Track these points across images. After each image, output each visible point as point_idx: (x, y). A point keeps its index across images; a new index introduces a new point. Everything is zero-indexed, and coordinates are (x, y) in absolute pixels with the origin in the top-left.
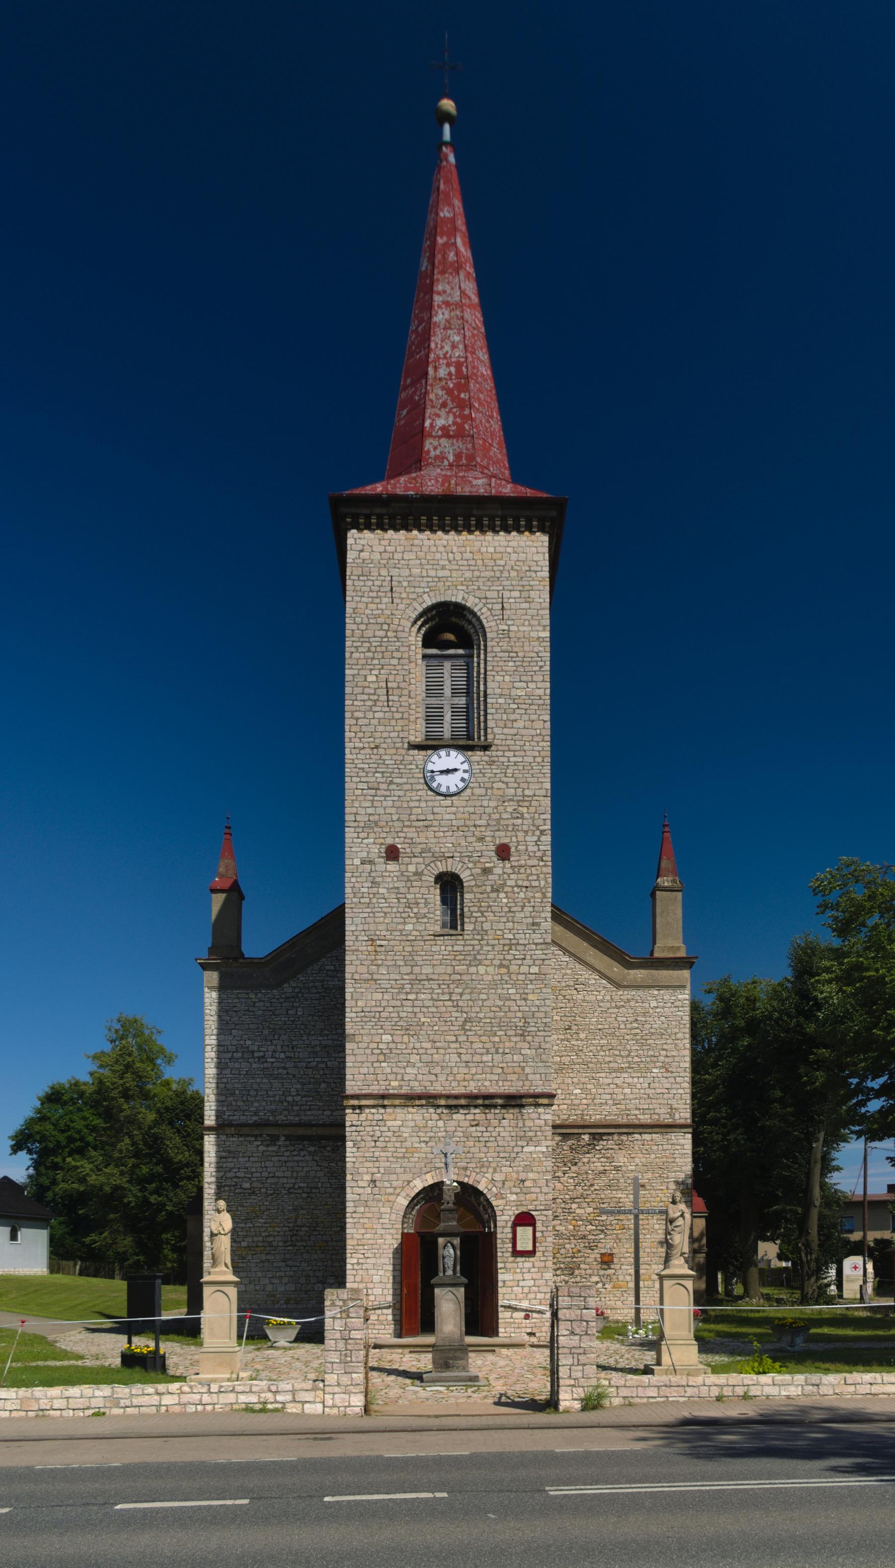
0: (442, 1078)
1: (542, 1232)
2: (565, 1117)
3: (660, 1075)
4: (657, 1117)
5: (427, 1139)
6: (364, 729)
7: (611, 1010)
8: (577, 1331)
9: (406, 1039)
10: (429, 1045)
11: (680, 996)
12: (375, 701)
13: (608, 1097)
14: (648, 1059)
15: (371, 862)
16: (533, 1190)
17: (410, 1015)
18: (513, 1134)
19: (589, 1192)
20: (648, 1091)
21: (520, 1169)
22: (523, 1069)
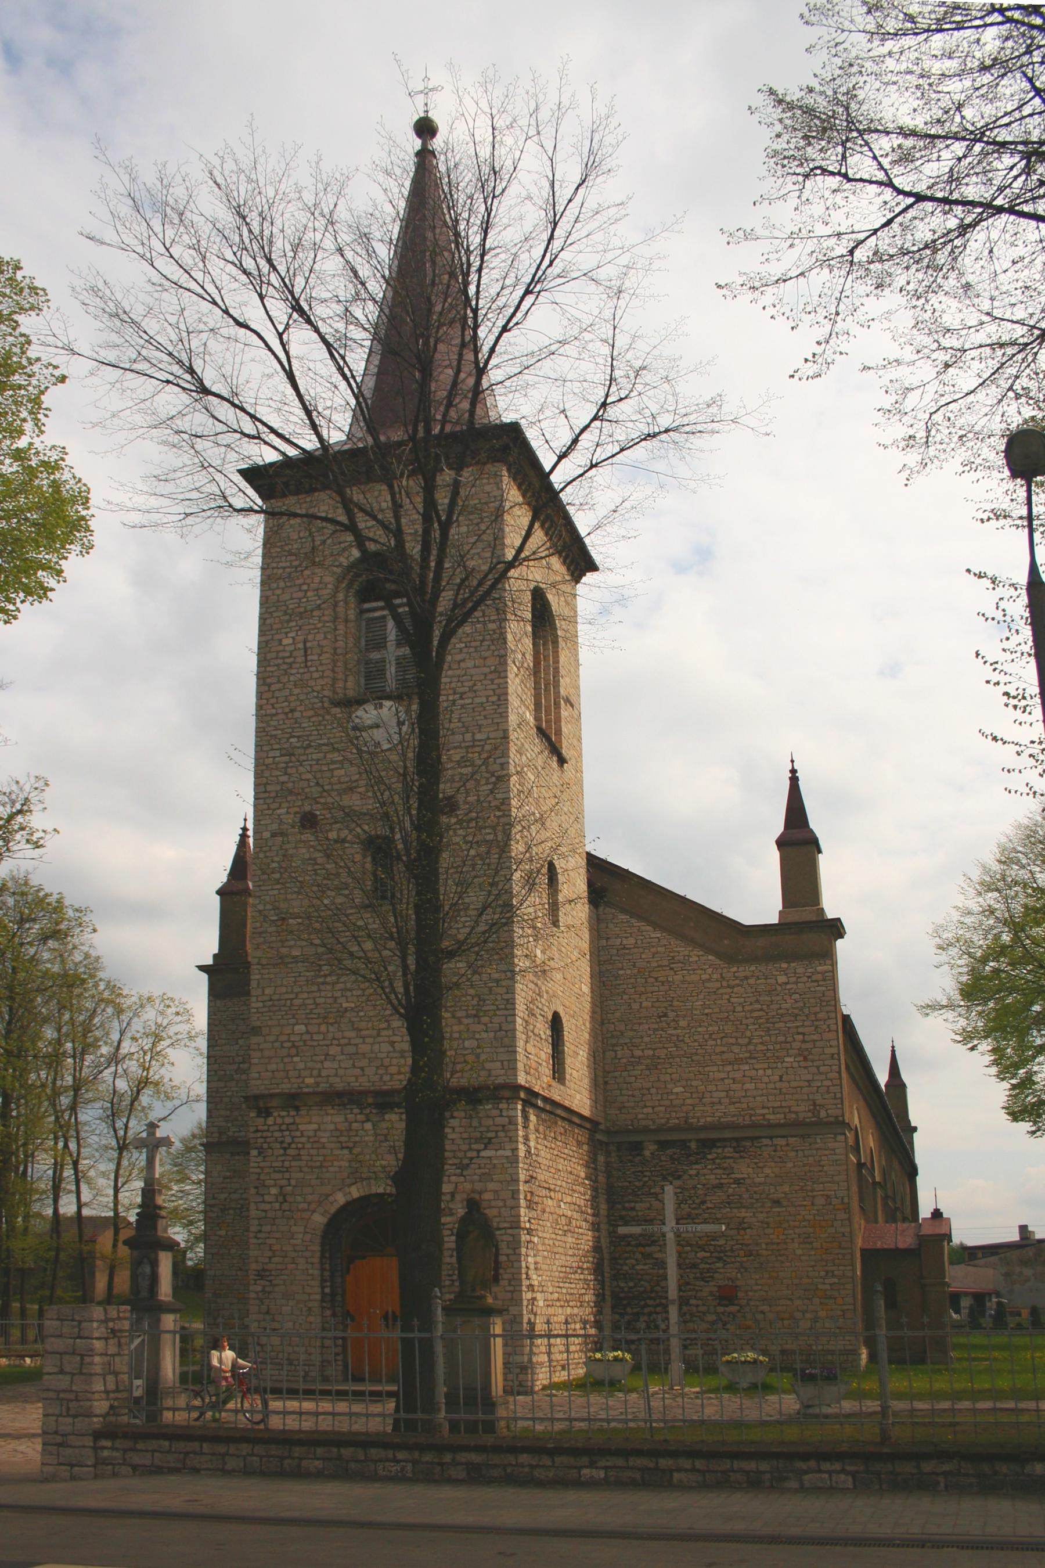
0: (369, 1071)
1: (508, 1255)
2: (663, 1121)
3: (795, 1065)
4: (793, 1116)
5: (351, 1145)
6: (277, 694)
7: (722, 991)
8: (67, 1369)
9: (323, 1028)
10: (353, 1034)
11: (819, 968)
12: (291, 664)
13: (724, 1094)
14: (778, 1047)
15: (283, 834)
16: (493, 1203)
17: (329, 1001)
18: (465, 1135)
19: (700, 1211)
20: (778, 1085)
21: (476, 1177)
22: (478, 1056)
